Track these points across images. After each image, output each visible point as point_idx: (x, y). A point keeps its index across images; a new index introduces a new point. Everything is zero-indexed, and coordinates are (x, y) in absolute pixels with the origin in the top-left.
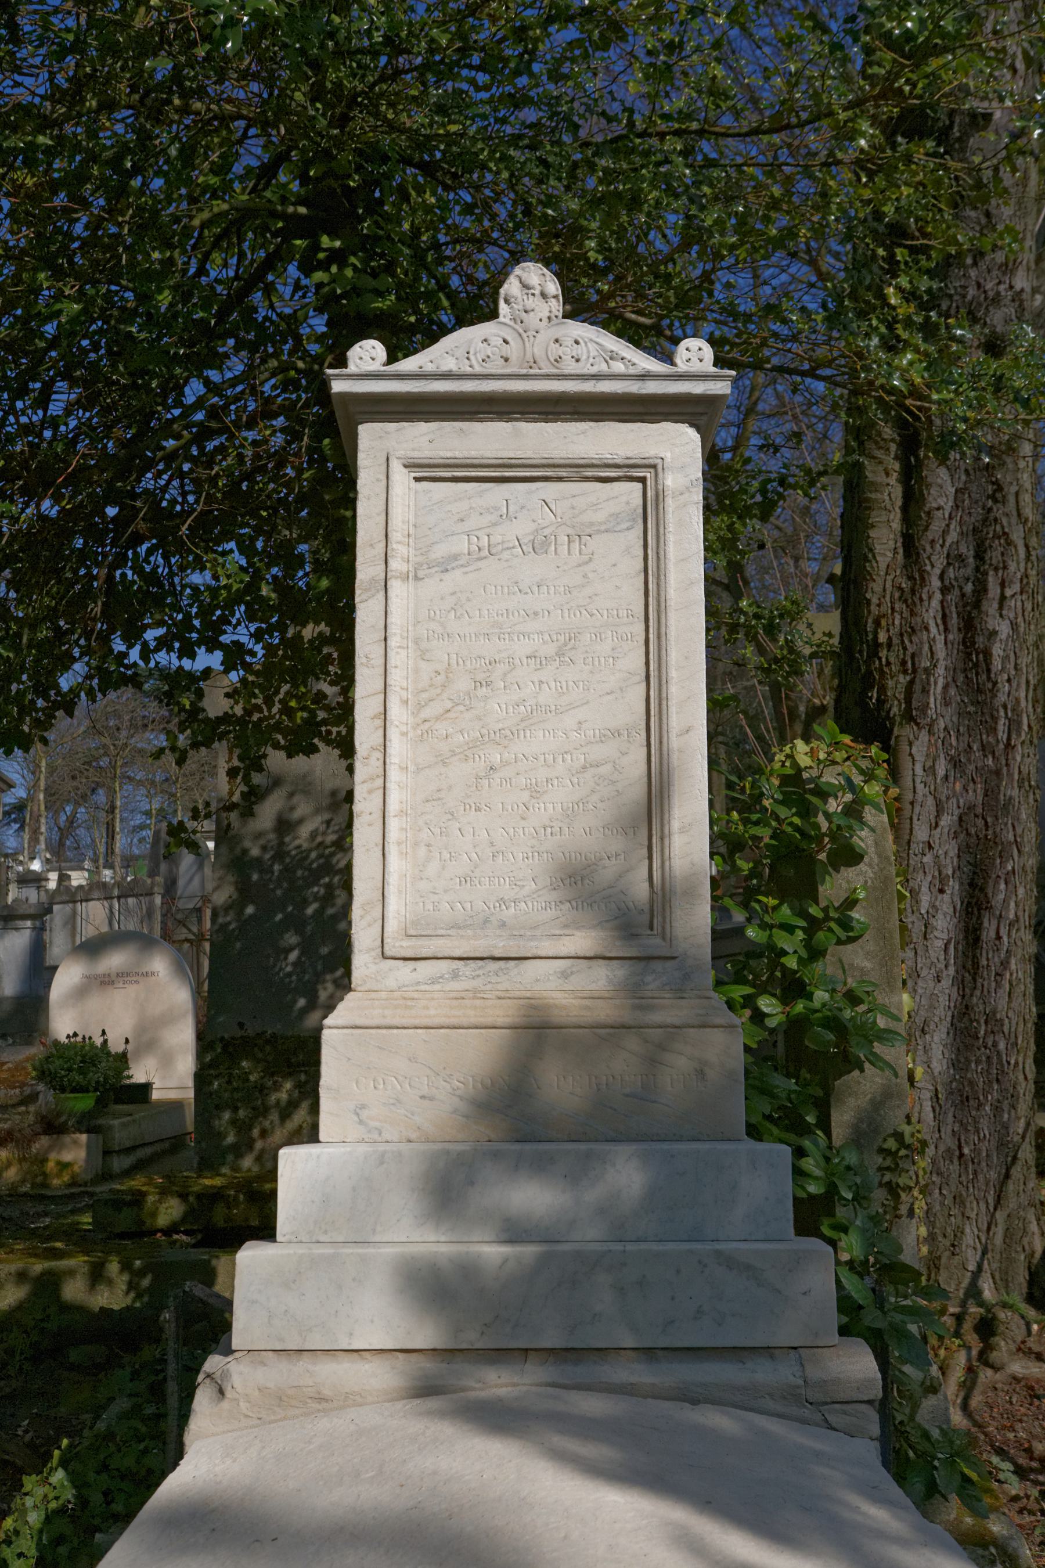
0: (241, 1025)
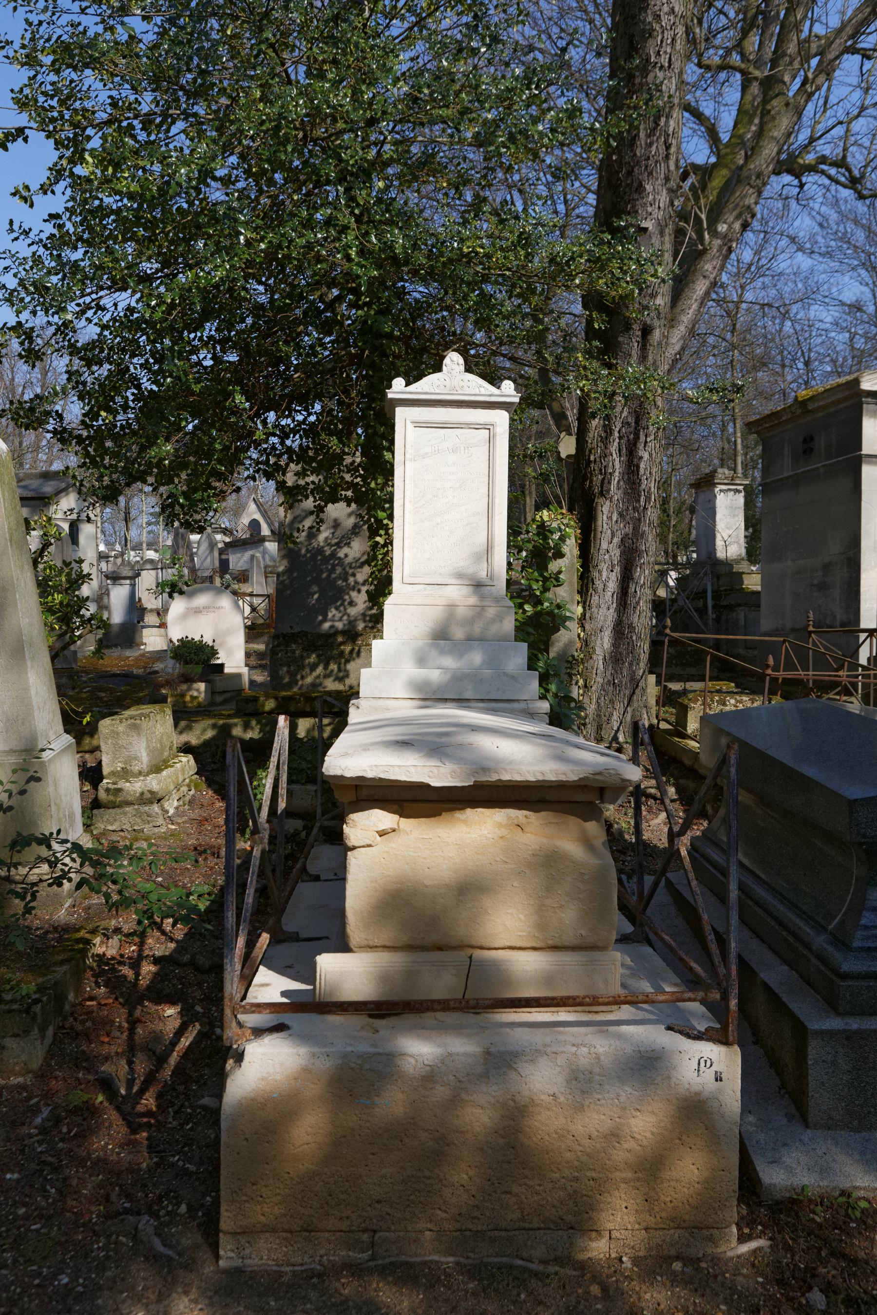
0: (291, 627)
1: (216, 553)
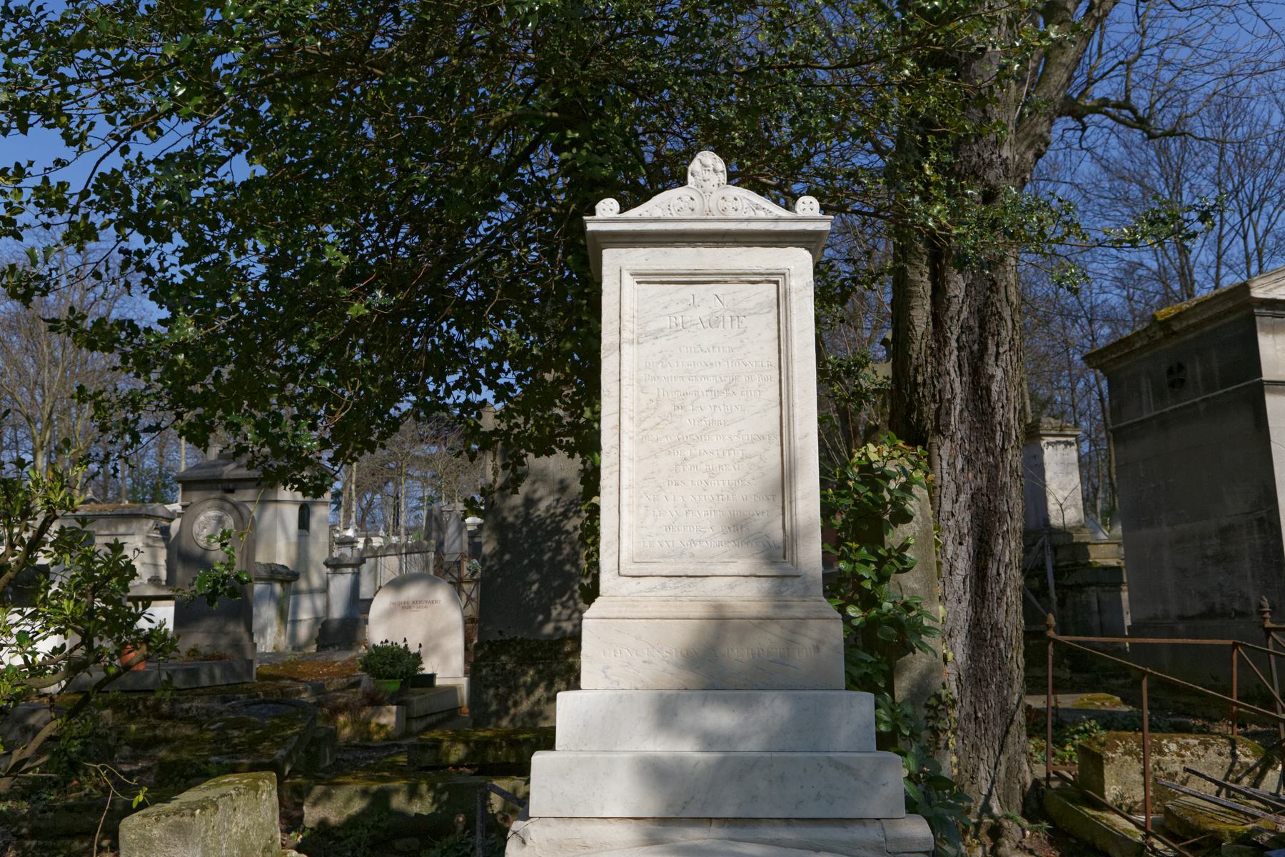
1: (465, 536)
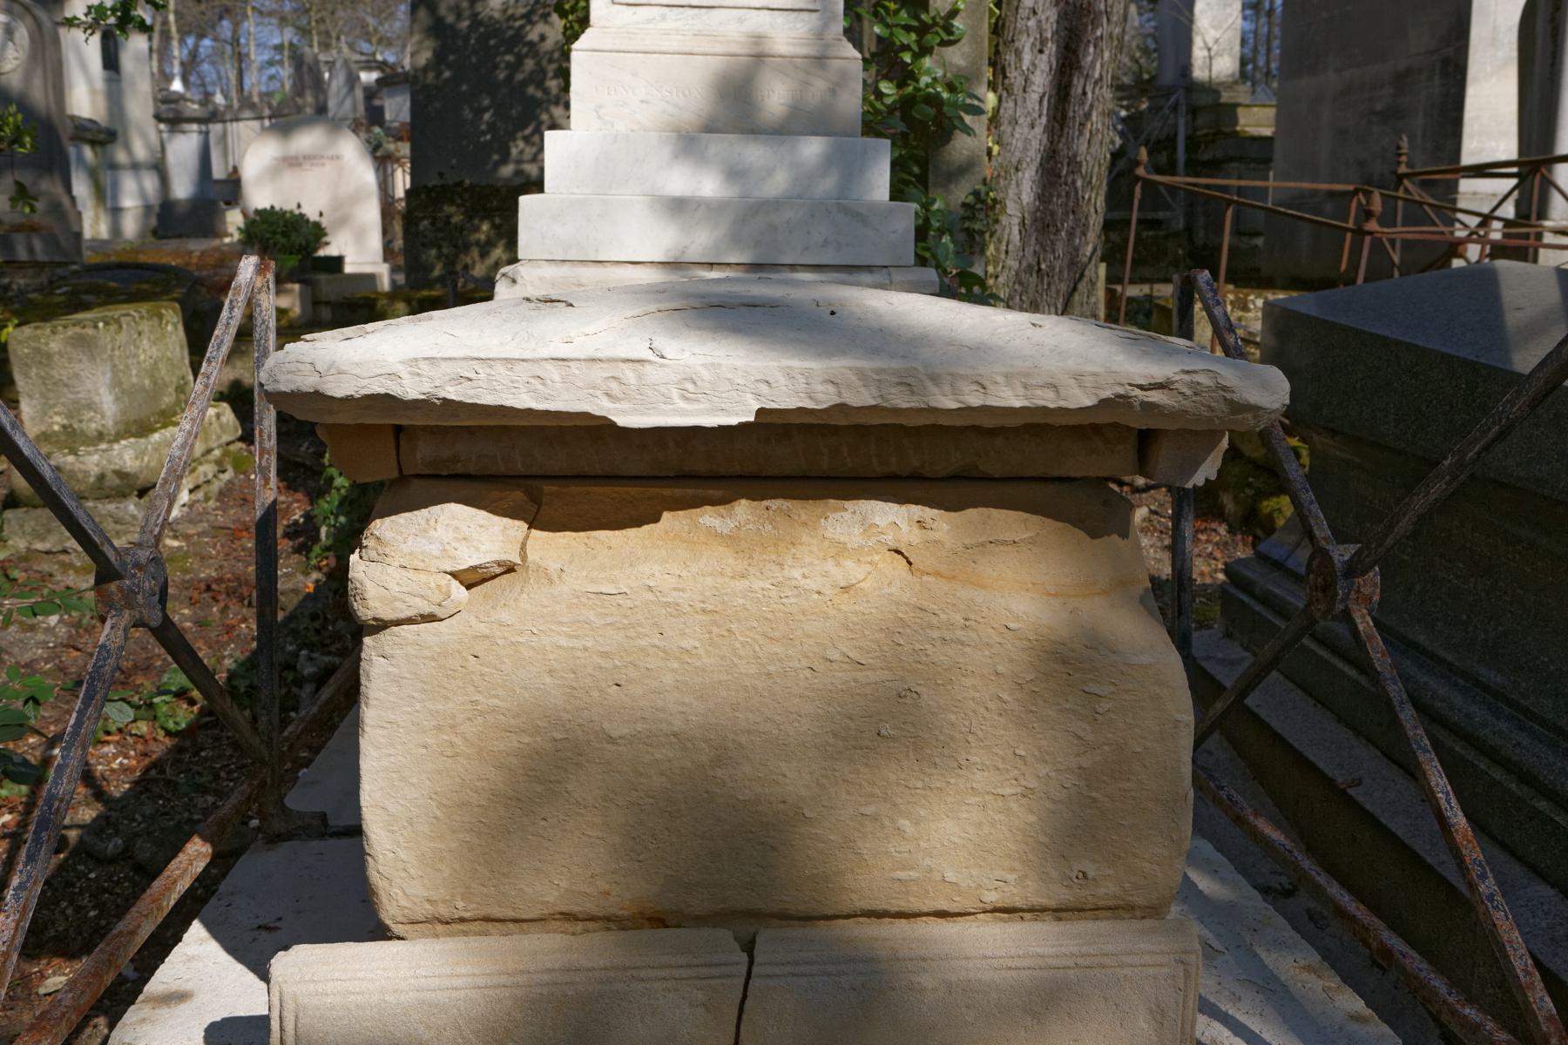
1: (359, 94)
